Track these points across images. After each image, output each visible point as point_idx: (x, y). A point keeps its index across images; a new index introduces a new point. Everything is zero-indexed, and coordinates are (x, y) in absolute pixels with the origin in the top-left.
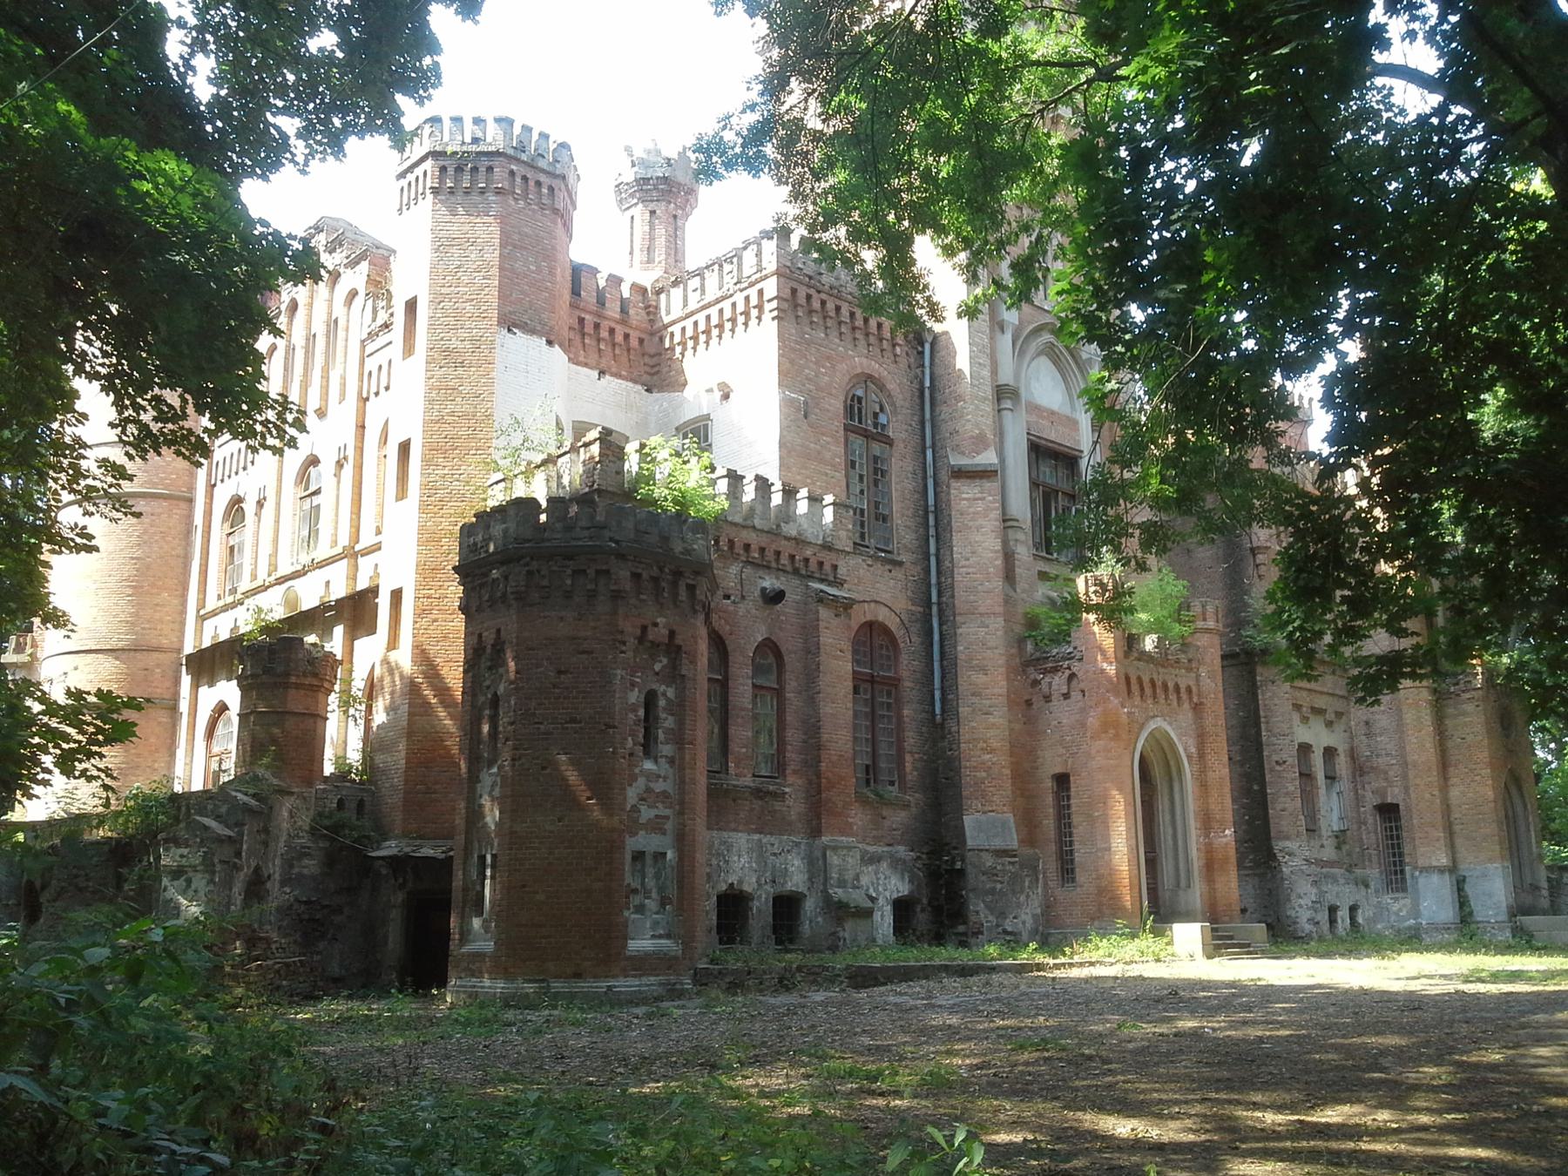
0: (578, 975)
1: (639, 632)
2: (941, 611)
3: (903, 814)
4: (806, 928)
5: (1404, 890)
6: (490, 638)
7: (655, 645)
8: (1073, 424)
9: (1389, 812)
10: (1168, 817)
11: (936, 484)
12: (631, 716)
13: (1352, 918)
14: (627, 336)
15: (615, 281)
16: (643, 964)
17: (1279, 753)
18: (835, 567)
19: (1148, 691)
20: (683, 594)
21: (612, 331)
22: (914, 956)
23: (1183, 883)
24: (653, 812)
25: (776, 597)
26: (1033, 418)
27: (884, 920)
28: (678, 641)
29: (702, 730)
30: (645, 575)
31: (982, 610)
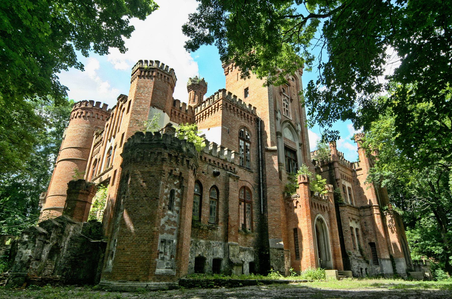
0: (138, 280)
1: (170, 171)
2: (263, 185)
3: (252, 238)
4: (222, 269)
5: (378, 264)
6: (126, 173)
7: (175, 176)
8: (295, 144)
9: (372, 245)
10: (323, 241)
11: (262, 154)
12: (165, 196)
13: (366, 271)
14: (187, 117)
15: (184, 104)
16: (160, 277)
17: (346, 229)
18: (234, 169)
19: (317, 206)
20: (185, 162)
21: (183, 116)
22: (253, 277)
23: (328, 259)
24: (170, 227)
25: (216, 174)
26: (285, 141)
27: (247, 267)
28: (183, 176)
29: (189, 205)
30: (173, 155)
31: (273, 184)
